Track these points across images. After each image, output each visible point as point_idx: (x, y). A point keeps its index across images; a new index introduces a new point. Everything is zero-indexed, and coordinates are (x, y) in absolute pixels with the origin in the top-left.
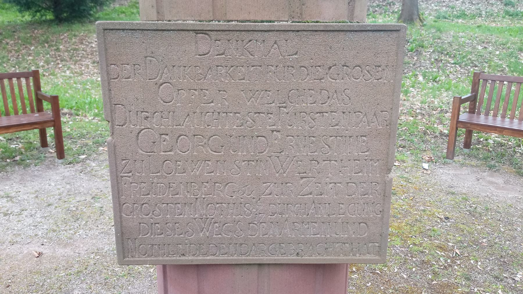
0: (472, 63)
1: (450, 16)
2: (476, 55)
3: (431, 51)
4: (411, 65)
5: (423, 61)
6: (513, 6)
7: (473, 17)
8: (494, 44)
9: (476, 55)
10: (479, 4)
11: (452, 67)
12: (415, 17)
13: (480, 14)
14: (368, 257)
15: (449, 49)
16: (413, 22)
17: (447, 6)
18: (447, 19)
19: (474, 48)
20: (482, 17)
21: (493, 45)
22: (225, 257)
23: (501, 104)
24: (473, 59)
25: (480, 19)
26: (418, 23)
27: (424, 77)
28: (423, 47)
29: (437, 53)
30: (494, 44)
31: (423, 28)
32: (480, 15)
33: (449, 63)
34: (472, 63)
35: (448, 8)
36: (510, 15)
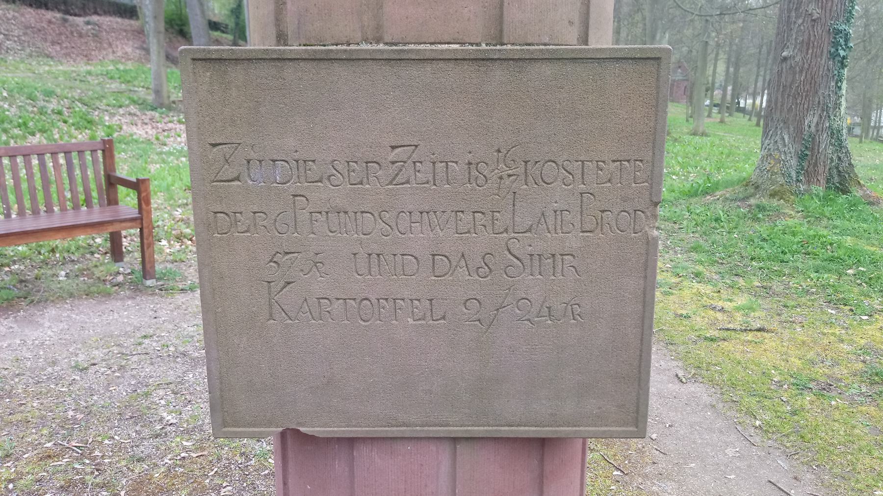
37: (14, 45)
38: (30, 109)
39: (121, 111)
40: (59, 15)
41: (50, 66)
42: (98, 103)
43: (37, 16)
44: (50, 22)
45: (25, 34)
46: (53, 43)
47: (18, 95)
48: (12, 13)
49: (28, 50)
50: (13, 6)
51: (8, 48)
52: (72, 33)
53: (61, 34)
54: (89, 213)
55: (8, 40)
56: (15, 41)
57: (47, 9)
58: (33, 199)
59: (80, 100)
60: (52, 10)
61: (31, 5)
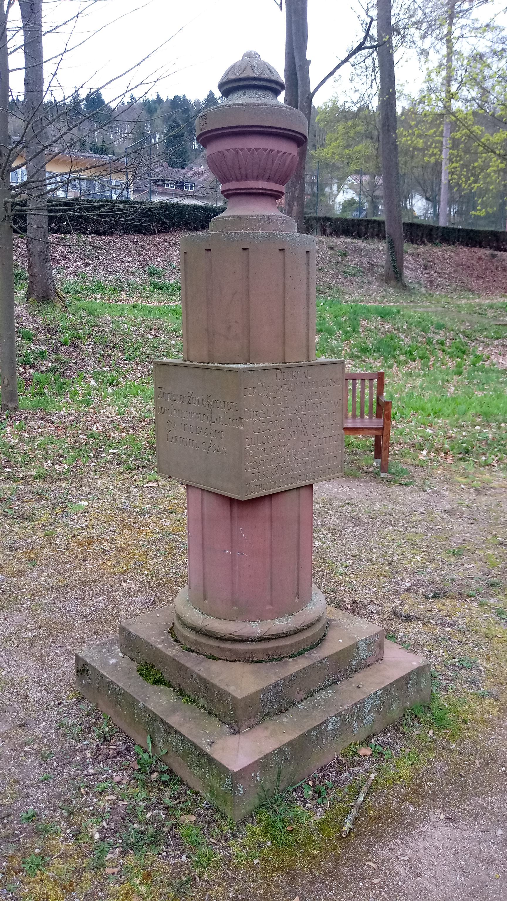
0: (148, 357)
1: (82, 289)
2: (149, 346)
3: (92, 343)
4: (72, 364)
5: (86, 358)
6: (160, 277)
7: (114, 291)
8: (166, 331)
9: (149, 346)
10: (116, 272)
11: (125, 364)
12: (52, 294)
13: (122, 287)
14: (338, 474)
15: (115, 340)
16: (51, 301)
17: (75, 275)
18: (81, 293)
19: (143, 337)
20: (125, 291)
21: (164, 333)
22: (286, 486)
23: (358, 412)
24: (148, 352)
25: (123, 293)
26: (59, 305)
27: (97, 380)
28: (79, 338)
29: (100, 347)
30: (166, 331)
31: (67, 310)
32: (123, 289)
33: (121, 359)
34: (148, 357)
35: (76, 278)
36: (159, 289)
37: (444, 282)
38: (420, 339)
39: (496, 342)
40: (488, 252)
41: (468, 299)
42: (478, 335)
43: (470, 255)
44: (480, 259)
45: (455, 271)
46: (478, 278)
47: (414, 328)
48: (449, 253)
49: (454, 286)
50: (452, 247)
51: (438, 285)
52: (497, 267)
53: (487, 269)
54: (362, 421)
55: (440, 277)
56: (445, 278)
57: (480, 247)
58: (354, 410)
59: (464, 333)
60: (485, 247)
61: (467, 245)
